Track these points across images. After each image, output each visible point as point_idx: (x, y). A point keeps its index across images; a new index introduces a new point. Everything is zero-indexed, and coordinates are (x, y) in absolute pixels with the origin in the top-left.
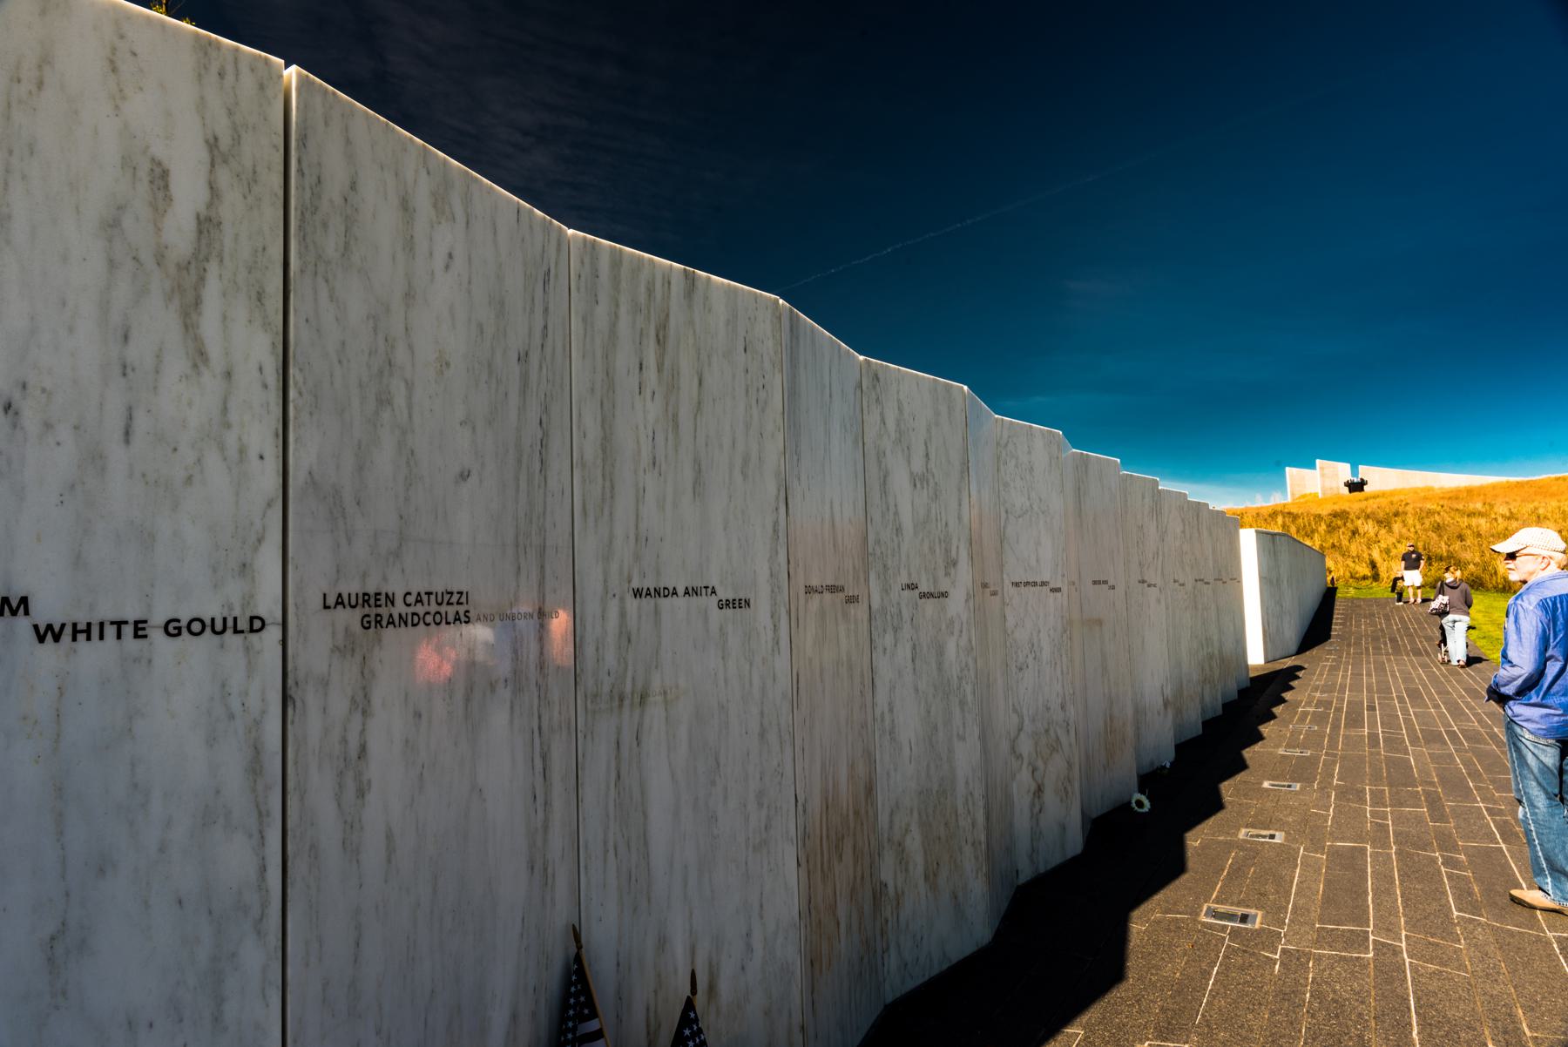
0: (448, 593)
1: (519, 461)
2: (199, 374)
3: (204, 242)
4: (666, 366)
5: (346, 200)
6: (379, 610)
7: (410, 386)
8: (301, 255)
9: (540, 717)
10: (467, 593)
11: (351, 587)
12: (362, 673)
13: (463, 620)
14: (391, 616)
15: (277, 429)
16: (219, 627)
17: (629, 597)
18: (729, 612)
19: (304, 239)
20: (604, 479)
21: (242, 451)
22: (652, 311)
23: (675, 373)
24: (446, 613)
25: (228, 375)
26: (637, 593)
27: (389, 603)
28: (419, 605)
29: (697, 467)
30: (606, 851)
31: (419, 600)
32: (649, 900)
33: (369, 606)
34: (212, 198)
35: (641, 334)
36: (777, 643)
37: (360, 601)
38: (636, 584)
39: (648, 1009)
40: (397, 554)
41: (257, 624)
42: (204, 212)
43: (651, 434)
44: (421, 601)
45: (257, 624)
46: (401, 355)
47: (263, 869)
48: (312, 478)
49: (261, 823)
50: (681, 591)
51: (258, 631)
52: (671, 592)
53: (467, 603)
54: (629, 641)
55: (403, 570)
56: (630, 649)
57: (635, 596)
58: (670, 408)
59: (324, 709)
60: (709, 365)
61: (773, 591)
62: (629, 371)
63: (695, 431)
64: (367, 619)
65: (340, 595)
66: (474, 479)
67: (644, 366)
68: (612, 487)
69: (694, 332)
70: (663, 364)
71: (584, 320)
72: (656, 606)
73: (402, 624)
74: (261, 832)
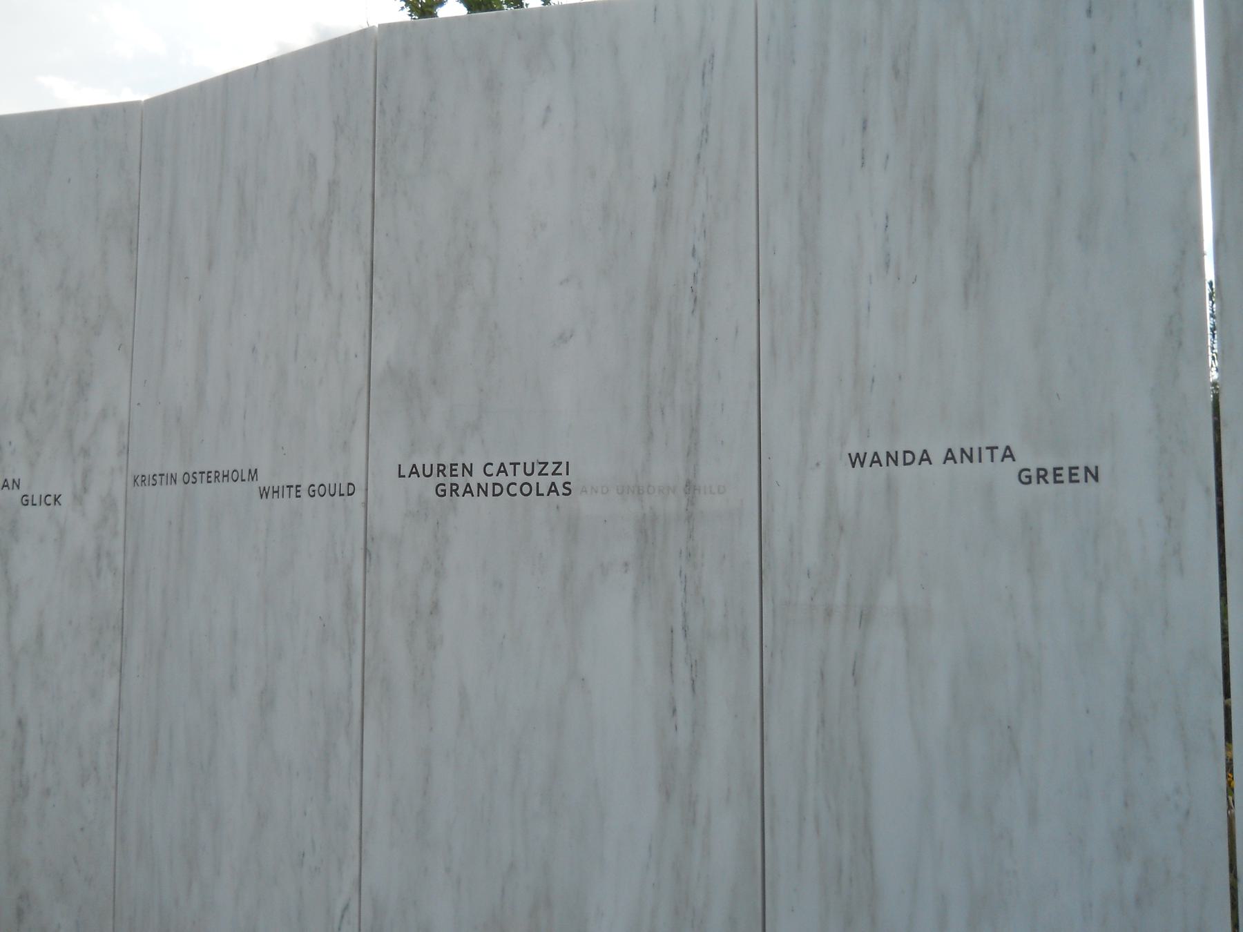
6: (454, 480)
9: (685, 615)
11: (427, 459)
13: (560, 493)
14: (468, 485)
18: (1047, 490)
26: (857, 460)
31: (502, 470)
47: (350, 686)
50: (937, 455)
51: (498, 495)
52: (918, 458)
53: (567, 474)
54: (842, 529)
55: (483, 441)
65: (414, 466)
68: (816, 312)
74: (350, 655)
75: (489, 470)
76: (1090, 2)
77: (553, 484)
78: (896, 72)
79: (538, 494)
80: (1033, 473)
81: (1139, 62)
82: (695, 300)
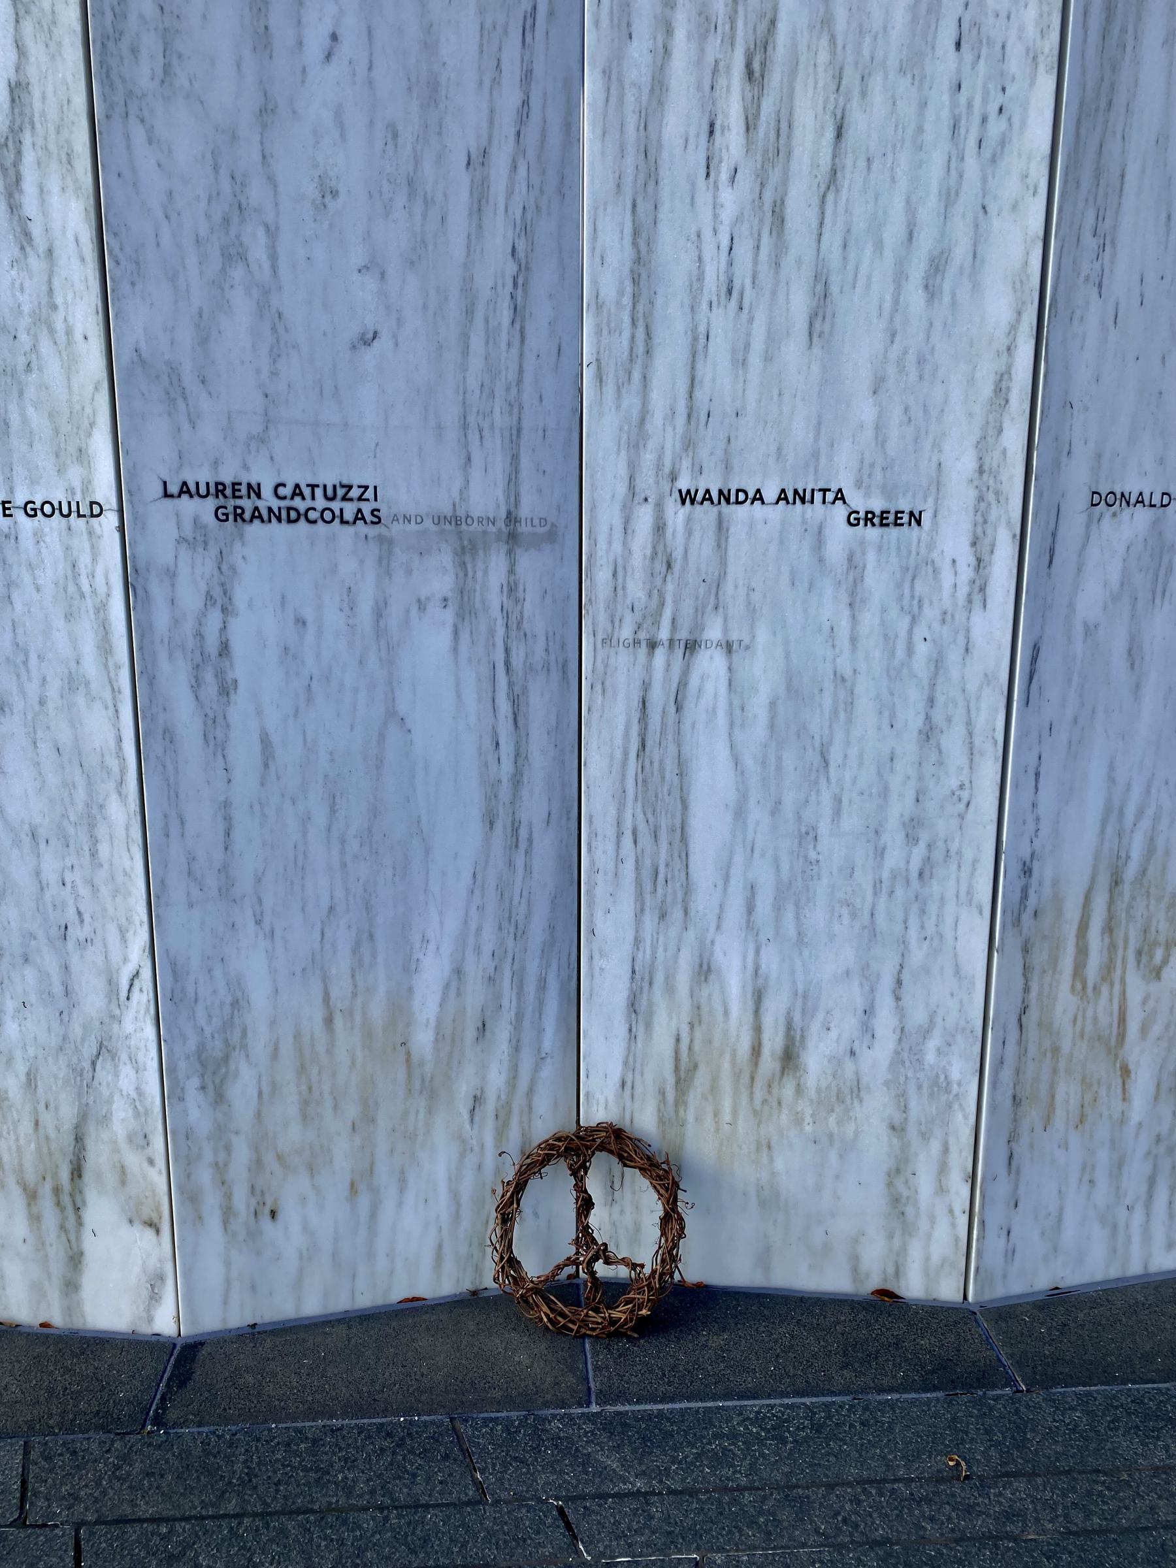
0: (343, 486)
1: (469, 312)
2: (26, 256)
3: (16, 111)
4: (763, 118)
5: (162, 8)
6: (239, 502)
7: (272, 232)
8: (104, 97)
9: (507, 650)
10: (375, 488)
11: (202, 475)
12: (219, 568)
15: (97, 305)
16: (65, 511)
17: (672, 503)
18: (872, 533)
19: (108, 76)
20: (634, 323)
21: (69, 332)
22: (740, 24)
23: (784, 127)
24: (341, 510)
25: (50, 252)
26: (687, 498)
27: (252, 494)
28: (298, 499)
29: (819, 288)
30: (620, 835)
31: (297, 491)
32: (686, 912)
33: (225, 497)
34: (19, 58)
35: (715, 71)
36: (982, 589)
37: (212, 490)
38: (684, 484)
39: (678, 1040)
40: (262, 439)
41: (96, 510)
42: (13, 78)
43: (725, 243)
44: (301, 495)
45: (95, 510)
46: (257, 192)
47: (120, 740)
48: (140, 356)
49: (114, 698)
50: (770, 494)
52: (751, 495)
53: (376, 500)
54: (669, 566)
56: (669, 578)
57: (683, 502)
58: (768, 196)
59: (172, 600)
60: (864, 94)
61: (981, 499)
62: (687, 141)
63: (821, 224)
64: (29, 506)
65: (185, 484)
66: (384, 343)
67: (717, 127)
68: (648, 335)
69: (833, 39)
70: (757, 115)
71: (607, 73)
72: (720, 513)
73: (273, 519)
75: (281, 491)
76: (550, 2)
77: (360, 511)
78: (750, 73)
79: (79, 516)
80: (862, 515)
81: (1001, 110)
82: (515, 309)
